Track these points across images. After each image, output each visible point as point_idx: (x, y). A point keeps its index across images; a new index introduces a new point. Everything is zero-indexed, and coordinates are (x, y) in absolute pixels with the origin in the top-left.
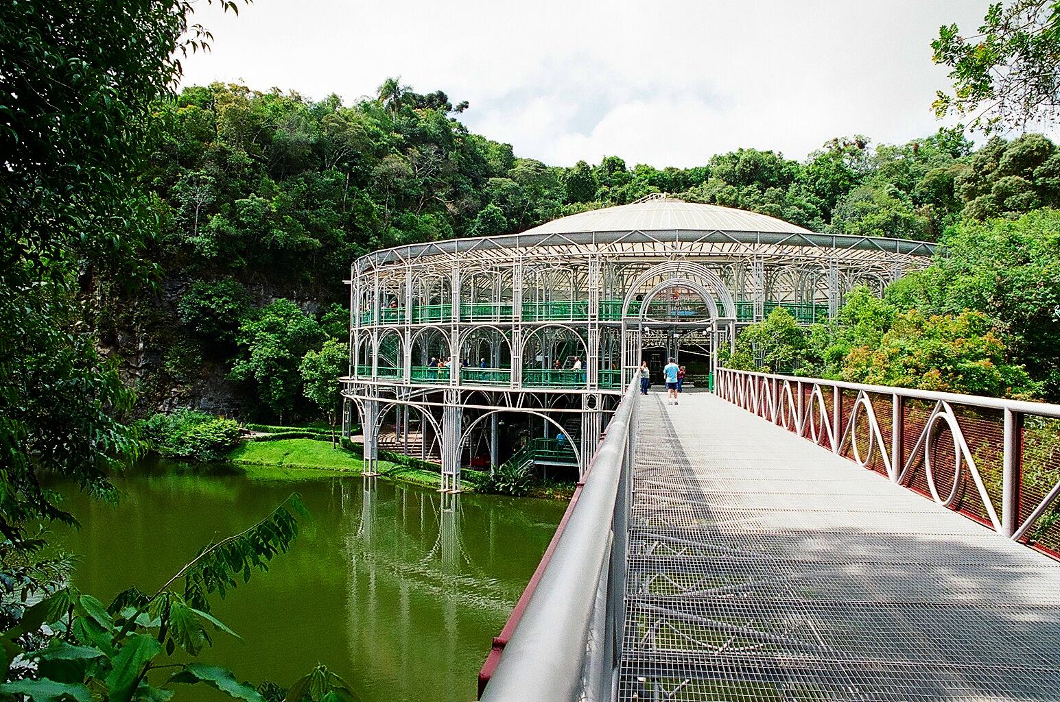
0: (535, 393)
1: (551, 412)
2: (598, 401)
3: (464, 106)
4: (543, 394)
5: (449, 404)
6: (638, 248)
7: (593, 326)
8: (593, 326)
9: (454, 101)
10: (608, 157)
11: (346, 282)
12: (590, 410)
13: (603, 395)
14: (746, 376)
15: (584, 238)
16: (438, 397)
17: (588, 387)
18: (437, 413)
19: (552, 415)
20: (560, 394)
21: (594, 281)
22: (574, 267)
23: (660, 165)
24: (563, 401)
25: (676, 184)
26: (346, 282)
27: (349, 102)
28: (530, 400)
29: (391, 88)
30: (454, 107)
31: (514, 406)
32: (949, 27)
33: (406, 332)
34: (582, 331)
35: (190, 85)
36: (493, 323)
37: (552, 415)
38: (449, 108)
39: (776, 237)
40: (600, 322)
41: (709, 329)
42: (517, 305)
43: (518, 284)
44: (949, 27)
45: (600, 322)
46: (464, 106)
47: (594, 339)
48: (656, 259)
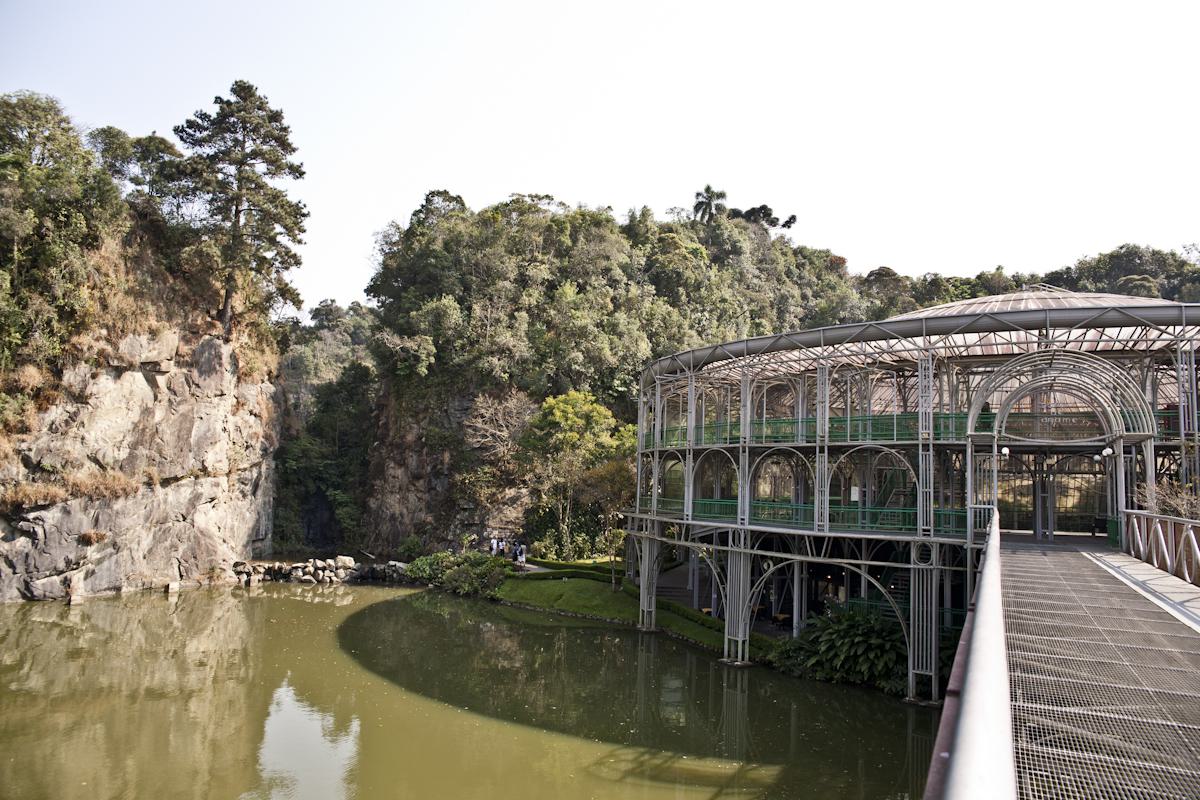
0: (851, 539)
1: (870, 566)
2: (934, 555)
3: (793, 219)
4: (860, 540)
5: (735, 549)
7: (926, 447)
8: (926, 447)
9: (781, 213)
12: (922, 566)
13: (942, 545)
16: (723, 538)
17: (920, 531)
18: (722, 559)
19: (872, 571)
20: (882, 541)
24: (885, 550)
25: (1056, 279)
28: (837, 547)
31: (819, 555)
32: (638, 214)
33: (688, 456)
35: (316, 305)
36: (791, 444)
37: (872, 571)
38: (774, 222)
39: (954, 322)
40: (920, 446)
41: (1107, 451)
44: (638, 214)
45: (920, 446)
47: (928, 463)
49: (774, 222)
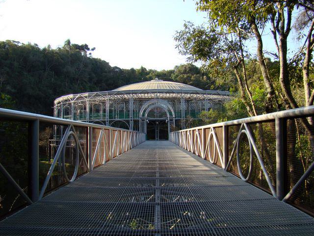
3: (93, 49)
6: (146, 95)
8: (107, 121)
9: (90, 47)
10: (72, 42)
11: (52, 107)
14: (186, 131)
15: (128, 92)
21: (131, 106)
22: (126, 101)
23: (159, 69)
25: (165, 76)
26: (52, 107)
27: (54, 47)
29: (142, 67)
30: (90, 49)
34: (128, 122)
38: (88, 49)
42: (107, 113)
43: (108, 105)
46: (93, 49)
48: (148, 99)
49: (88, 49)
